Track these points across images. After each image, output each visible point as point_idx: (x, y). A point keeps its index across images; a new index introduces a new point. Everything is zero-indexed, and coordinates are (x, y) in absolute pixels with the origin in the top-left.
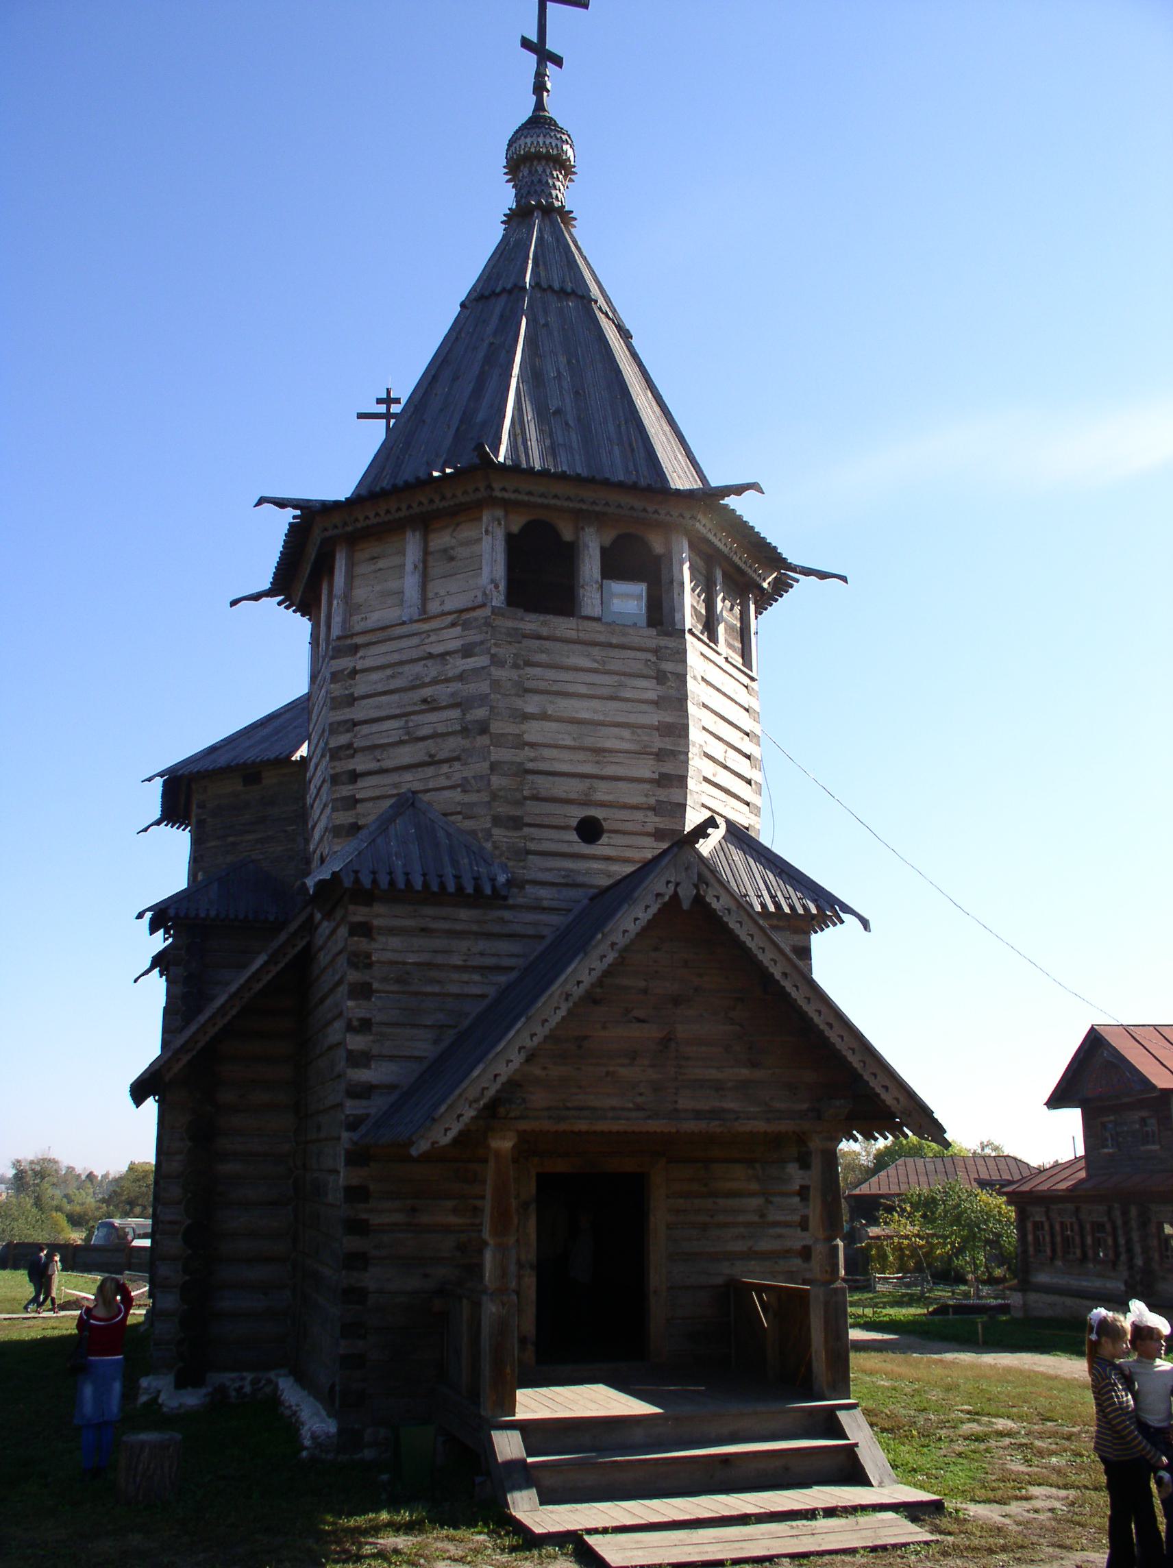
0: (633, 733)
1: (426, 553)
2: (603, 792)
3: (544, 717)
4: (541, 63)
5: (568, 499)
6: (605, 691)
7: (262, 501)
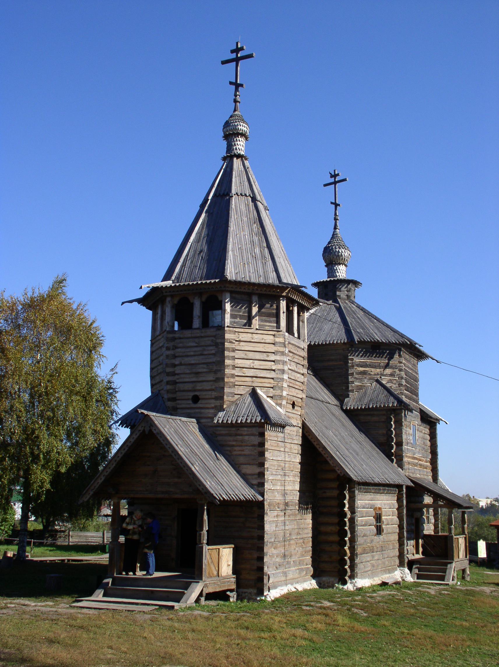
0: (207, 366)
2: (199, 387)
3: (181, 364)
4: (237, 90)
5: (185, 290)
6: (199, 353)
7: (123, 303)
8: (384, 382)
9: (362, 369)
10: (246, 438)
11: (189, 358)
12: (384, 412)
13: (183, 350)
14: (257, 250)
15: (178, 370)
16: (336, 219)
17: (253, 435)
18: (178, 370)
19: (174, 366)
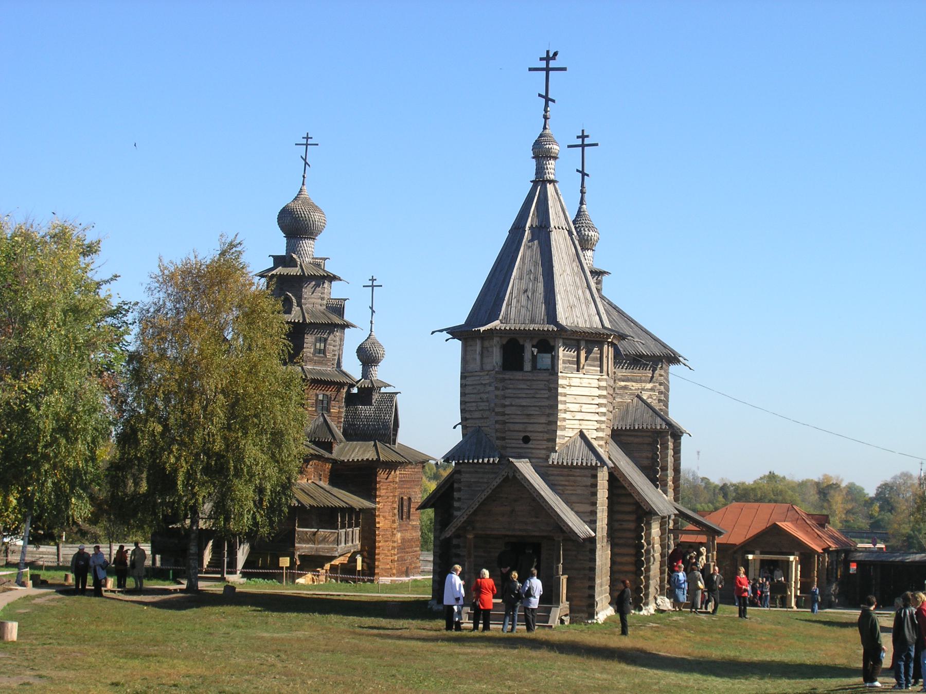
1: (482, 347)
2: (530, 428)
3: (511, 405)
4: (547, 105)
7: (433, 333)
8: (645, 398)
9: (623, 384)
10: (579, 479)
11: (521, 400)
12: (649, 434)
13: (514, 392)
14: (580, 292)
15: (508, 410)
16: (582, 192)
17: (585, 476)
18: (508, 410)
19: (505, 406)
